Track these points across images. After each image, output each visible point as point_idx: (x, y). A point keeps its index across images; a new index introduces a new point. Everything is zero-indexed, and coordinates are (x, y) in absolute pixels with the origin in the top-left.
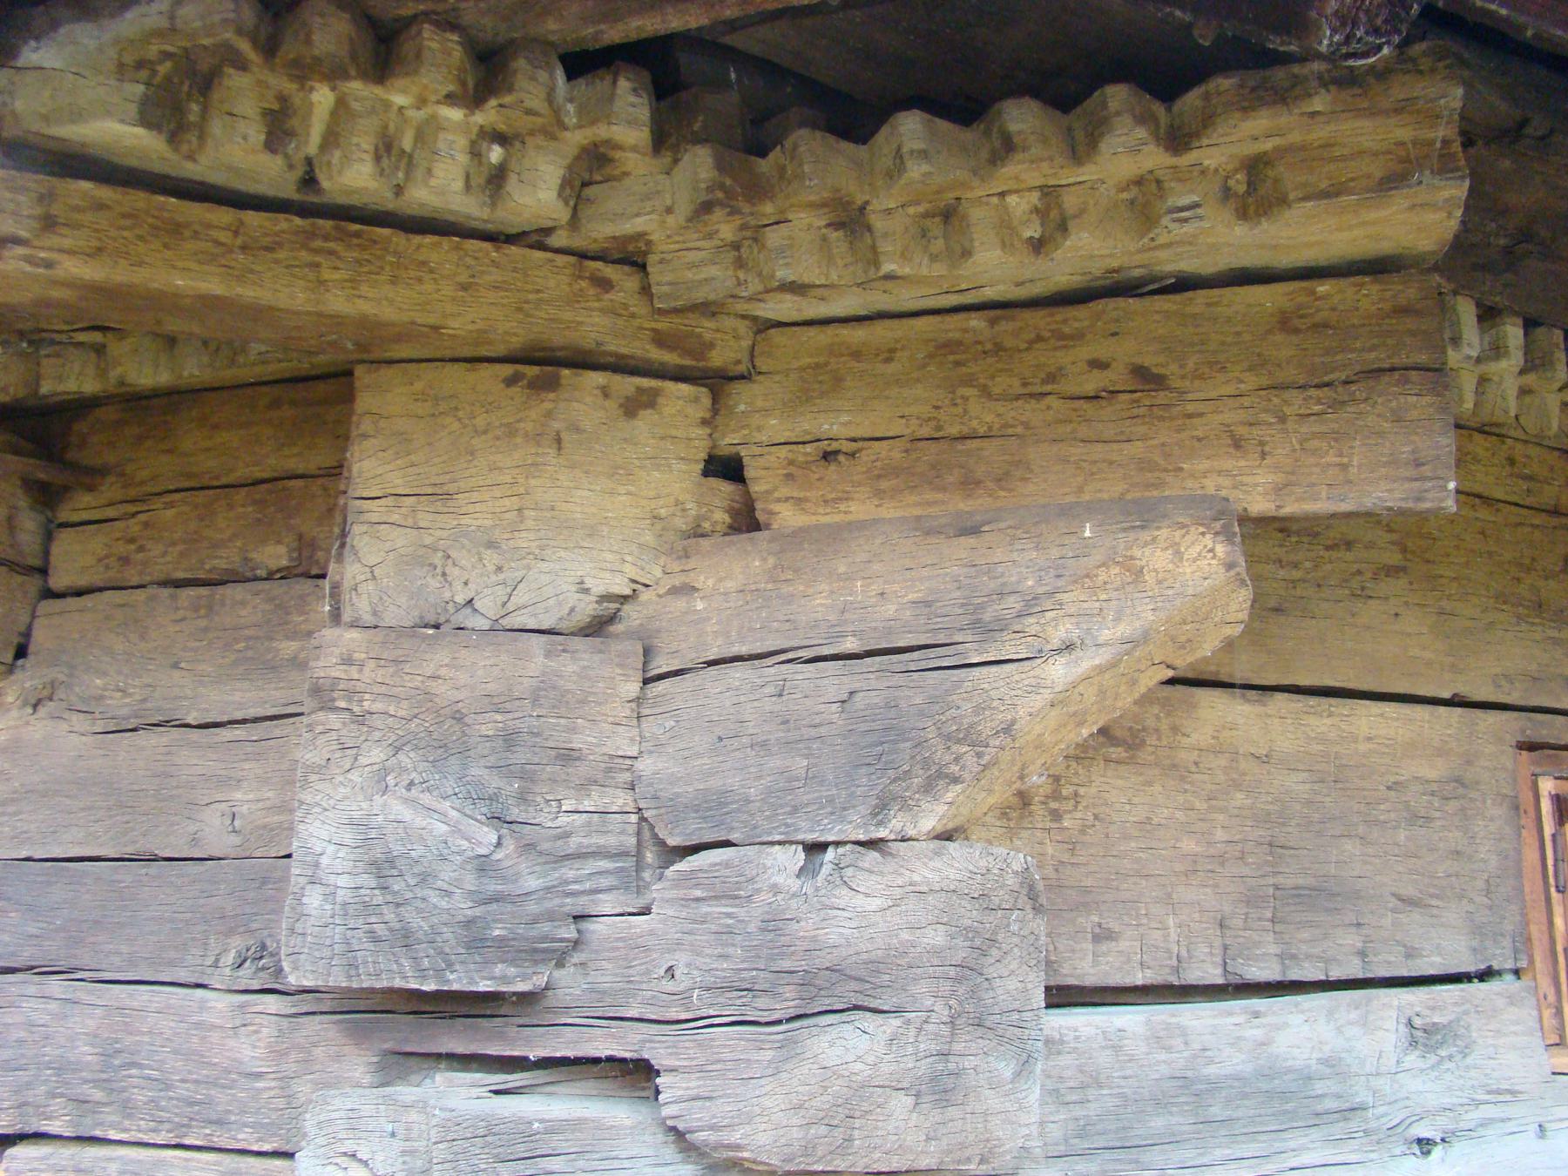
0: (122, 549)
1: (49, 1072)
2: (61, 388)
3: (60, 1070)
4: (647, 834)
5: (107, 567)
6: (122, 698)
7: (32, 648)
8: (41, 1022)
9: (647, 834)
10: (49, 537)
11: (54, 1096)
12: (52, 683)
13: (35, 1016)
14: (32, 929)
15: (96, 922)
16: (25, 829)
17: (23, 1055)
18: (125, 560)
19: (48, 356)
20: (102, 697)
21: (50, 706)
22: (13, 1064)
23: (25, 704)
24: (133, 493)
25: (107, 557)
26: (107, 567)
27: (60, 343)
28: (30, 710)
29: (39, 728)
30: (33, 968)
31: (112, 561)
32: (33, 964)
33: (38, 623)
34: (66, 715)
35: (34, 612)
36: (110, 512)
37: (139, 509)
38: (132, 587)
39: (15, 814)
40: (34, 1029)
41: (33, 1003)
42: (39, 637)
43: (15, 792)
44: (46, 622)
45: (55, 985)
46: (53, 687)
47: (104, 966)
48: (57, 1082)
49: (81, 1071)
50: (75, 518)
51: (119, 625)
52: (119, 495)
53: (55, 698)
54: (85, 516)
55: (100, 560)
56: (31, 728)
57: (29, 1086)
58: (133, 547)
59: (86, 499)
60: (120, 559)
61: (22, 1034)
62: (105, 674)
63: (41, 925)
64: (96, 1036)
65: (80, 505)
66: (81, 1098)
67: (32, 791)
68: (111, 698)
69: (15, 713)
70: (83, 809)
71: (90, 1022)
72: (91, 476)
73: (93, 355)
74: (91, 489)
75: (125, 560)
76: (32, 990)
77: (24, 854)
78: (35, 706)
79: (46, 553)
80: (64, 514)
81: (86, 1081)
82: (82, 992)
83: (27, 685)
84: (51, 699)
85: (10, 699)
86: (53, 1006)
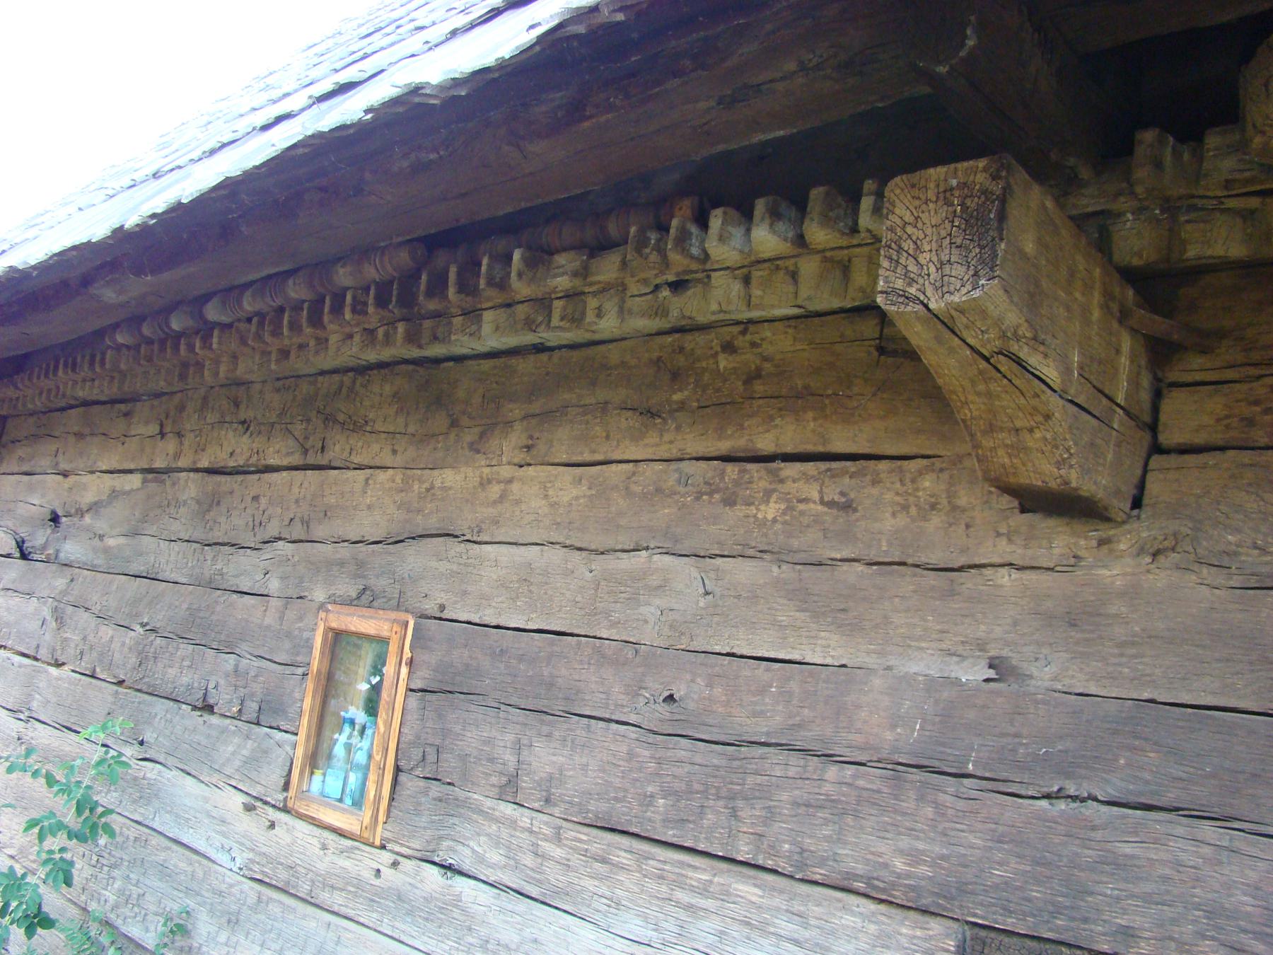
0: (1247, 411)
1: (1197, 913)
2: (1209, 252)
3: (1210, 914)
4: (355, 603)
5: (1228, 427)
6: (1260, 556)
7: (1146, 501)
8: (1191, 863)
9: (355, 603)
10: (1157, 395)
11: (1204, 937)
12: (1175, 535)
13: (1183, 856)
14: (1177, 771)
15: (1255, 775)
16: (1148, 672)
17: (1168, 892)
18: (1250, 422)
19: (1188, 222)
20: (1236, 554)
21: (1174, 557)
22: (1156, 898)
23: (1141, 551)
24: (1256, 356)
25: (1227, 417)
26: (1228, 427)
27: (1202, 209)
28: (1148, 559)
29: (1160, 578)
30: (1177, 809)
31: (1234, 422)
32: (1180, 805)
33: (1149, 477)
34: (1196, 567)
35: (1146, 464)
36: (1230, 374)
37: (1263, 372)
38: (1260, 448)
39: (1135, 657)
40: (1181, 869)
41: (1181, 844)
42: (1154, 486)
43: (1133, 636)
44: (1161, 476)
45: (1208, 830)
46: (1176, 539)
47: (1267, 821)
48: (1208, 925)
49: (1237, 919)
50: (1188, 378)
51: (1250, 485)
52: (1240, 358)
53: (1179, 549)
54: (1198, 377)
55: (1218, 420)
56: (1151, 577)
57: (1174, 921)
58: (1258, 409)
59: (1197, 361)
60: (1242, 419)
61: (1168, 871)
62: (1238, 530)
63: (1187, 769)
64: (1257, 888)
65: (1194, 366)
66: (1237, 945)
67: (1156, 637)
68: (1248, 555)
69: (1128, 560)
70: (1219, 660)
71: (1251, 874)
72: (1206, 342)
73: (1239, 221)
74: (1204, 351)
75: (1250, 422)
76: (1180, 831)
77: (1146, 696)
78: (1155, 555)
79: (1155, 410)
80: (1174, 375)
81: (1245, 931)
82: (1240, 841)
83: (1144, 535)
84: (1173, 549)
85: (1122, 546)
86: (1206, 850)
